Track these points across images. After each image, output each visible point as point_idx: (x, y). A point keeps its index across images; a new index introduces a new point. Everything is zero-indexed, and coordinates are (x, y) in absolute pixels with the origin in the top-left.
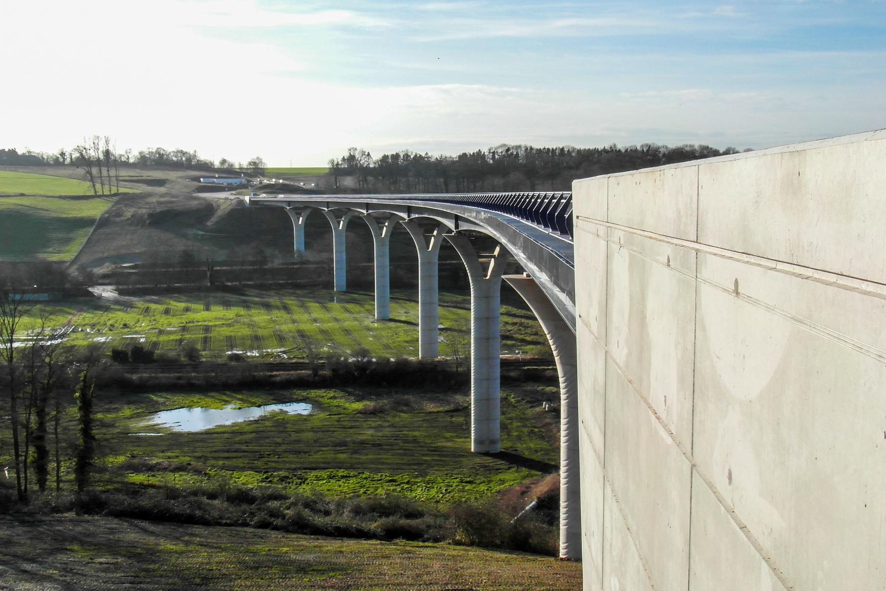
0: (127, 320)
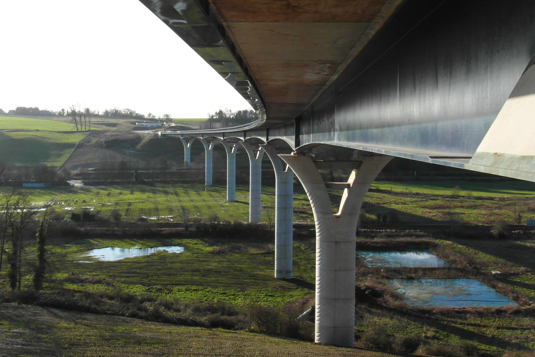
0: (86, 198)
